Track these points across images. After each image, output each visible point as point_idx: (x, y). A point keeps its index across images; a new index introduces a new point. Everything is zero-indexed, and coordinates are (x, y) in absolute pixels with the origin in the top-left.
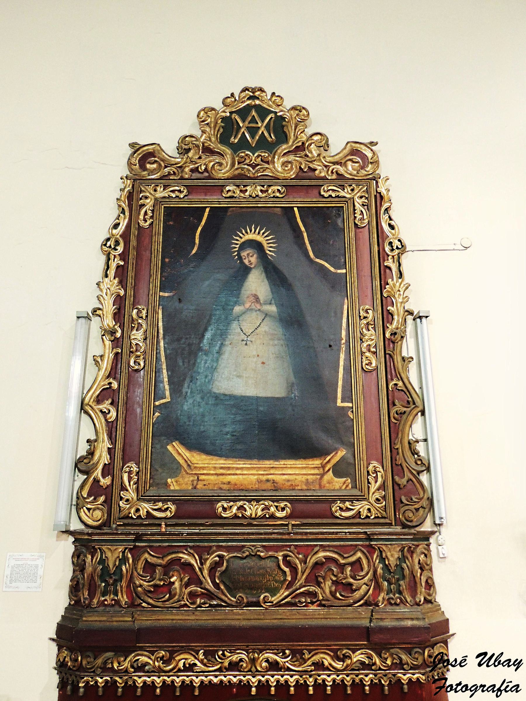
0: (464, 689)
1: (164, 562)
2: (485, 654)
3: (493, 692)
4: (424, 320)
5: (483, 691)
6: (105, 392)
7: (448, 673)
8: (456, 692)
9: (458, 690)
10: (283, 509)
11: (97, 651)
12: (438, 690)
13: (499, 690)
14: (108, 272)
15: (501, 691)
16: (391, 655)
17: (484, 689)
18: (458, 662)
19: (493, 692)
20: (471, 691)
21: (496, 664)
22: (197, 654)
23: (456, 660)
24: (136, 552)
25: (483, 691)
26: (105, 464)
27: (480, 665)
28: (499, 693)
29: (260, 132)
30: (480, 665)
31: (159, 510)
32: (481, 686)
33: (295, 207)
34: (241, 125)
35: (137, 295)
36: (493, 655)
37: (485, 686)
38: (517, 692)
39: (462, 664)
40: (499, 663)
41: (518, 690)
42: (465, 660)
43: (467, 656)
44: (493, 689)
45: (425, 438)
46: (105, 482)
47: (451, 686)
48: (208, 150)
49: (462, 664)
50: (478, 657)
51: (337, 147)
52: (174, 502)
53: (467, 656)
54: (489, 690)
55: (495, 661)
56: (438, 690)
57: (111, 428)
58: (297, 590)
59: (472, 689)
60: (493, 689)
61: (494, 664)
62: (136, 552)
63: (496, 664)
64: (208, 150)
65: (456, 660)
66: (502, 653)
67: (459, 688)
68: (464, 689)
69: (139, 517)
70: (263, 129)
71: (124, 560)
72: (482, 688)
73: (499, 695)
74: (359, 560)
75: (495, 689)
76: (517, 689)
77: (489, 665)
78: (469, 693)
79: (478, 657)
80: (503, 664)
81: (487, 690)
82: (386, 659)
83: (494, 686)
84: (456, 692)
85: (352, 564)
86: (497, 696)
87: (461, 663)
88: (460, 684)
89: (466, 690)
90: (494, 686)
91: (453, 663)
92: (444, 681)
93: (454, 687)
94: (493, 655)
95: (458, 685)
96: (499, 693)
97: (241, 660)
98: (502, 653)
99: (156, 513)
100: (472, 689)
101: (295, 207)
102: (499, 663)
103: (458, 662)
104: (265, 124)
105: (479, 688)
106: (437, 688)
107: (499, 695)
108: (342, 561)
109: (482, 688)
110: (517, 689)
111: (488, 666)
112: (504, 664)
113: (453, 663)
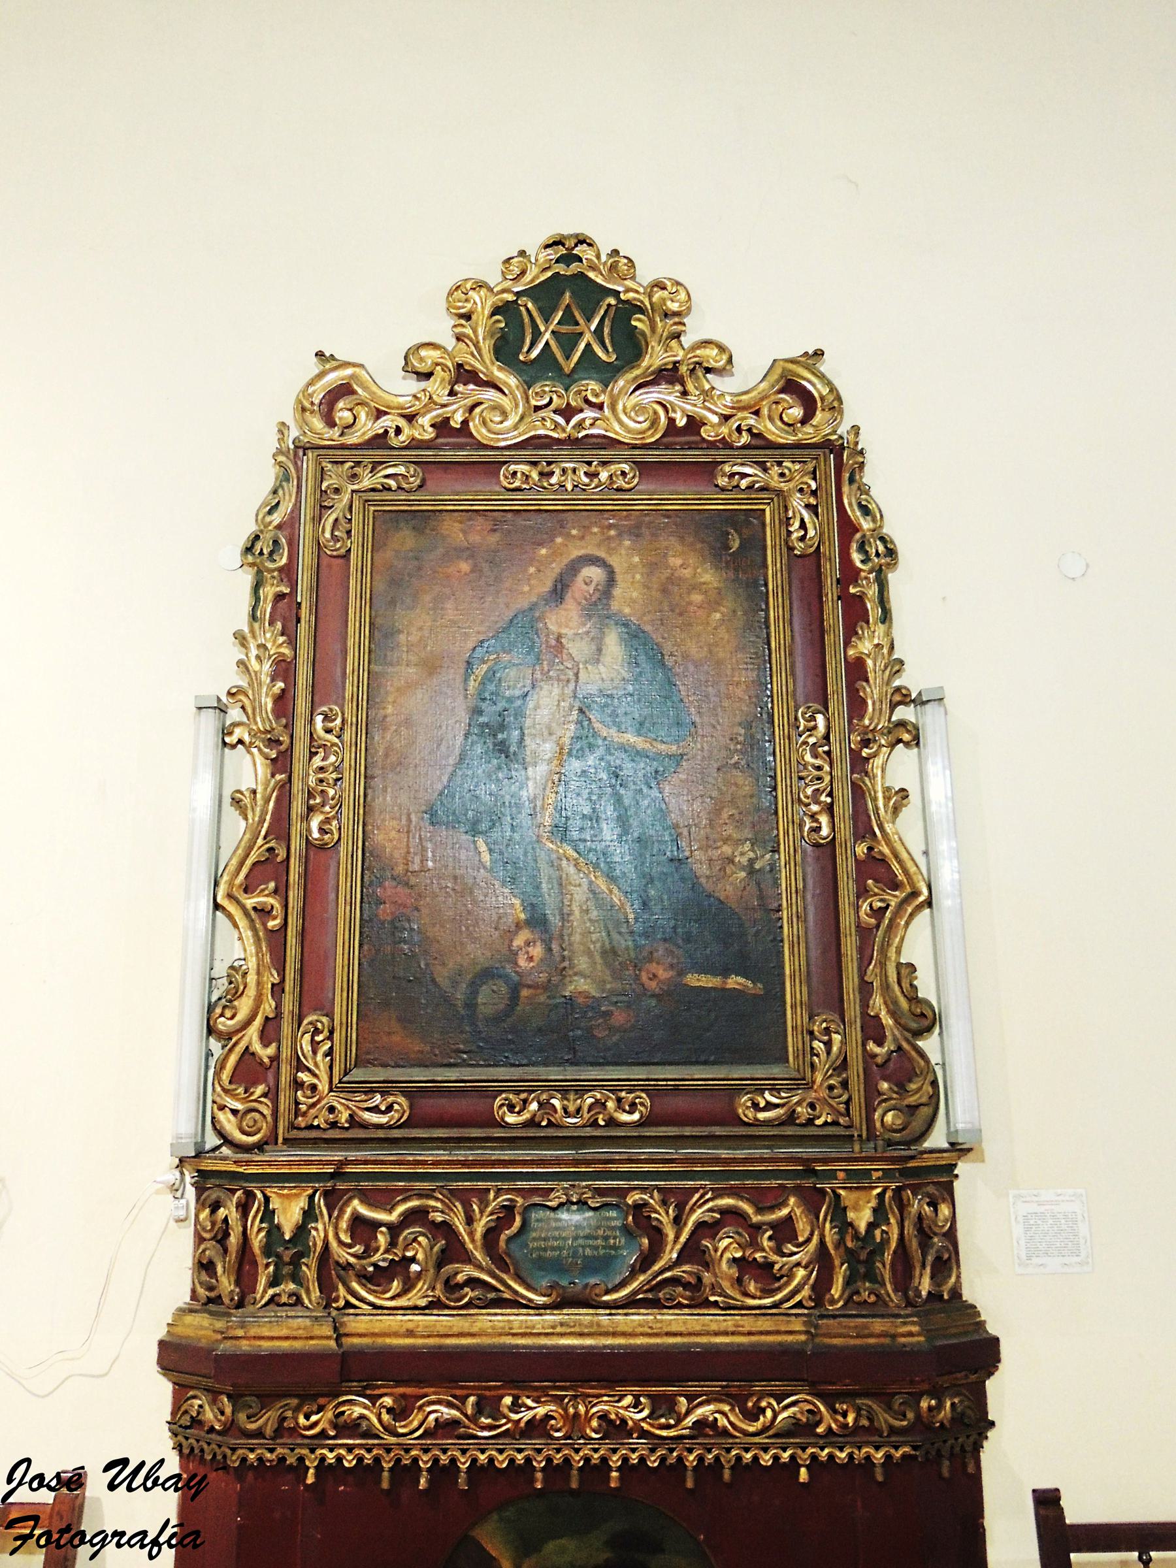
1: (393, 1217)
2: (124, 1462)
3: (143, 1546)
5: (119, 1545)
6: (259, 868)
9: (62, 1542)
10: (633, 1107)
11: (266, 1399)
12: (19, 1543)
13: (155, 1542)
15: (160, 1546)
16: (858, 1411)
17: (123, 1541)
19: (143, 1546)
20: (93, 1545)
21: (149, 1484)
22: (464, 1403)
24: (334, 1199)
25: (119, 1545)
26: (267, 1018)
27: (112, 1486)
28: (155, 1550)
29: (582, 346)
30: (112, 1486)
31: (375, 1110)
32: (115, 1534)
34: (542, 329)
35: (818, 680)
36: (143, 1464)
37: (123, 1534)
38: (196, 1546)
40: (155, 1483)
41: (198, 1542)
44: (142, 1540)
46: (265, 1053)
47: (41, 1477)
48: (464, 375)
50: (107, 1468)
51: (748, 375)
52: (405, 1093)
54: (132, 1542)
55: (147, 1478)
56: (19, 1543)
57: (276, 940)
58: (662, 1272)
59: (95, 1541)
60: (142, 1540)
61: (144, 1484)
62: (334, 1199)
63: (149, 1484)
64: (464, 375)
66: (162, 1461)
67: (67, 1536)
69: (334, 1125)
70: (588, 337)
71: (309, 1214)
72: (116, 1539)
73: (154, 1553)
74: (789, 1218)
75: (146, 1542)
76: (195, 1540)
77: (134, 1486)
79: (107, 1468)
80: (163, 1485)
81: (128, 1542)
82: (845, 1415)
83: (144, 1533)
85: (773, 1225)
86: (151, 1557)
90: (144, 1533)
91: (53, 1483)
92: (32, 1523)
93: (55, 1536)
94: (143, 1464)
96: (155, 1550)
97: (548, 1417)
98: (162, 1461)
99: (368, 1116)
100: (95, 1541)
102: (155, 1483)
104: (593, 328)
105: (109, 1538)
106: (16, 1539)
107: (154, 1553)
108: (756, 1219)
109: (116, 1539)
110: (195, 1540)
111: (130, 1489)
112: (167, 1485)
113: (53, 1483)
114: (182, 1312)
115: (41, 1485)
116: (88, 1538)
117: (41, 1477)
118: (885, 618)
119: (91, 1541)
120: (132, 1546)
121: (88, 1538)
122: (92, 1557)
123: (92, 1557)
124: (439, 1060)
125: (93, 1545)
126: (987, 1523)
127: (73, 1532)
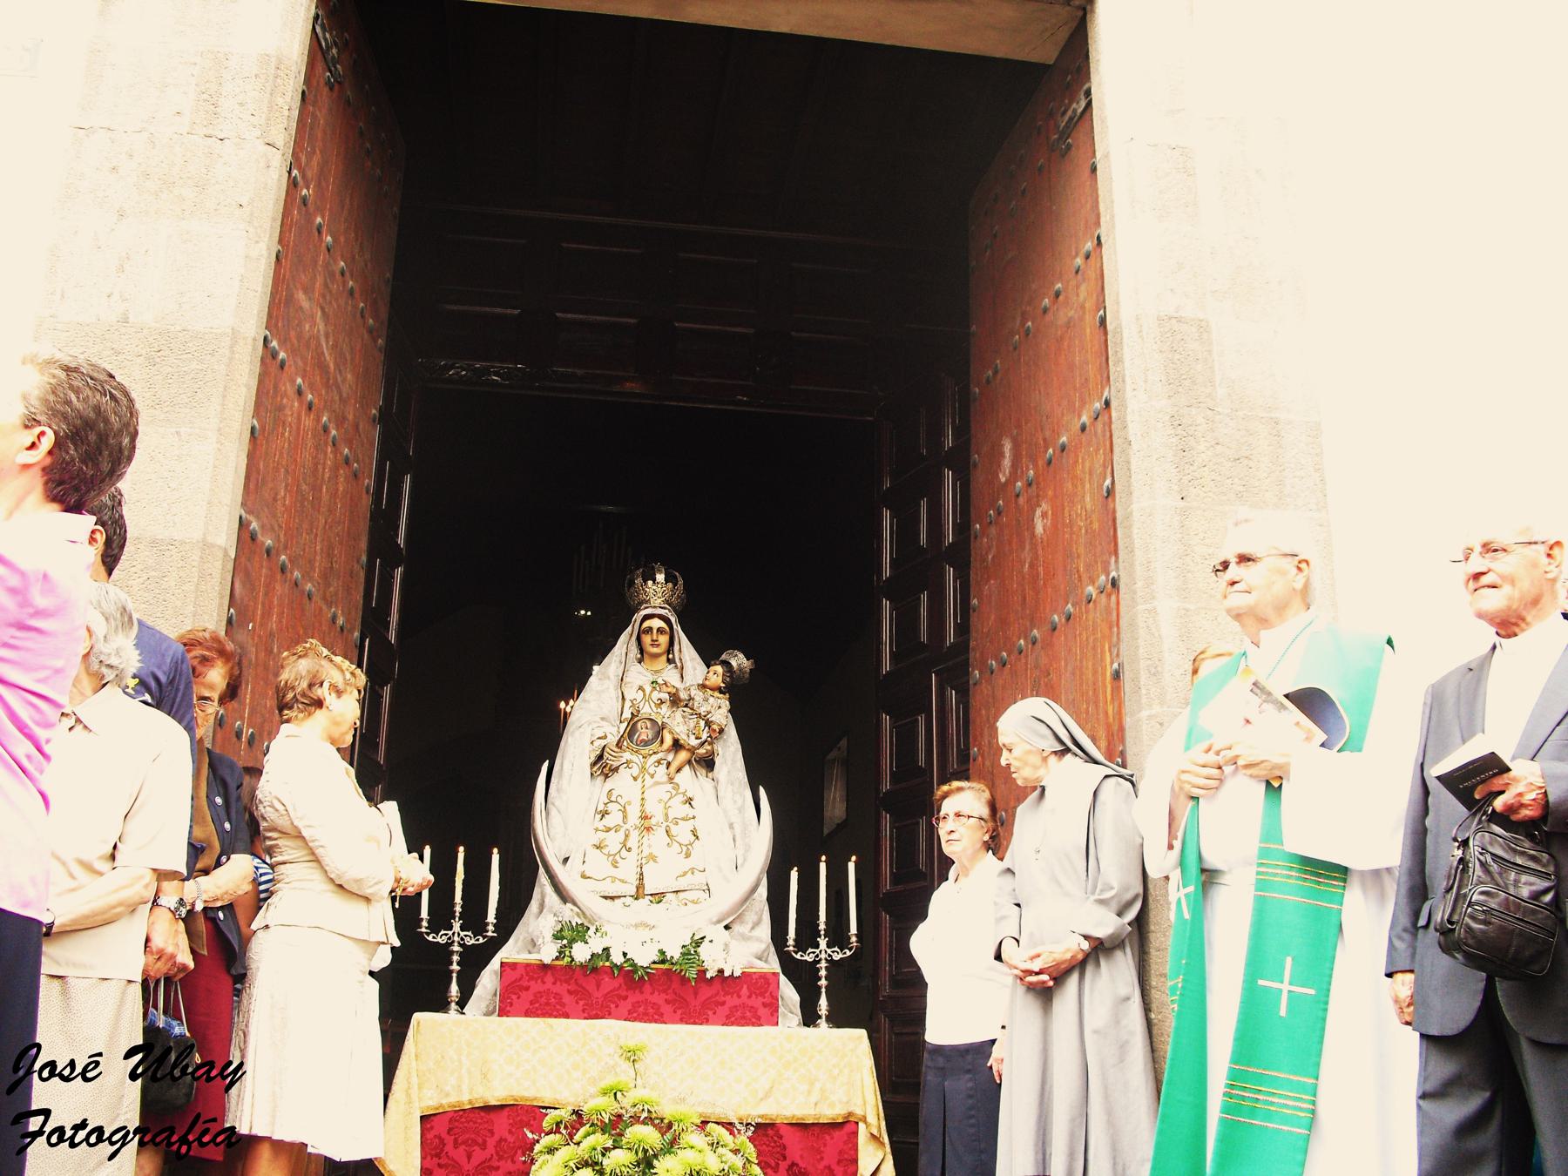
0: (93, 1139)
4: (79, 728)
7: (49, 768)
8: (73, 1145)
14: (1428, 822)
18: (79, 1070)
23: (72, 1064)
33: (677, 991)
36: (41, 772)
39: (89, 1075)
42: (97, 1064)
43: (100, 1054)
45: (131, 319)
47: (52, 1065)
49: (89, 1075)
50: (128, 1056)
53: (100, 1054)
65: (72, 1064)
67: (82, 1135)
68: (93, 1139)
78: (106, 1149)
79: (128, 1056)
81: (213, 1140)
84: (73, 1145)
87: (85, 1070)
88: (83, 1124)
89: (100, 1140)
91: (66, 1072)
92: (42, 1118)
93: (69, 1133)
95: (77, 1128)
101: (677, 991)
103: (79, 1070)
113: (66, 1072)
114: (260, 897)
115: (52, 1074)
116: (106, 1135)
117: (52, 1065)
118: (1122, 1047)
119: (109, 1138)
120: (217, 1145)
121: (106, 1135)
122: (111, 1157)
123: (111, 1157)
124: (254, 476)
125: (112, 1144)
126: (358, 1158)
127: (89, 1129)
